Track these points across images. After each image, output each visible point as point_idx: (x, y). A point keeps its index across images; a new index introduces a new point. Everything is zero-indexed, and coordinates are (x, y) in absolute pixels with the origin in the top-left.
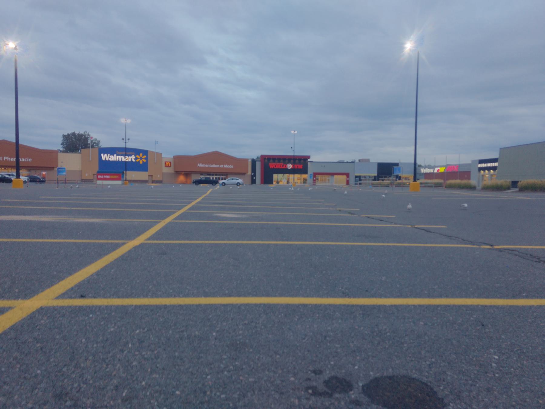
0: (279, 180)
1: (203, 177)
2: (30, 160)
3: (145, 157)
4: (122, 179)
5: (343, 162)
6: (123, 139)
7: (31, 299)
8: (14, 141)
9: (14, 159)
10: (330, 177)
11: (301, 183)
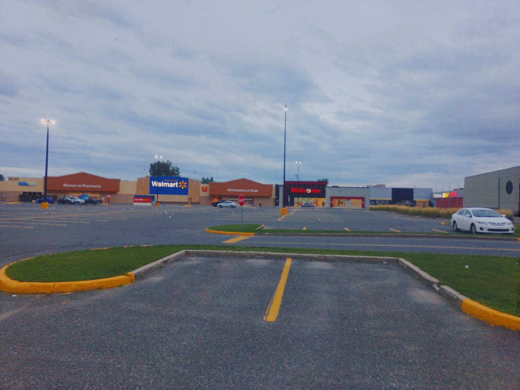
2: (100, 187)
3: (186, 183)
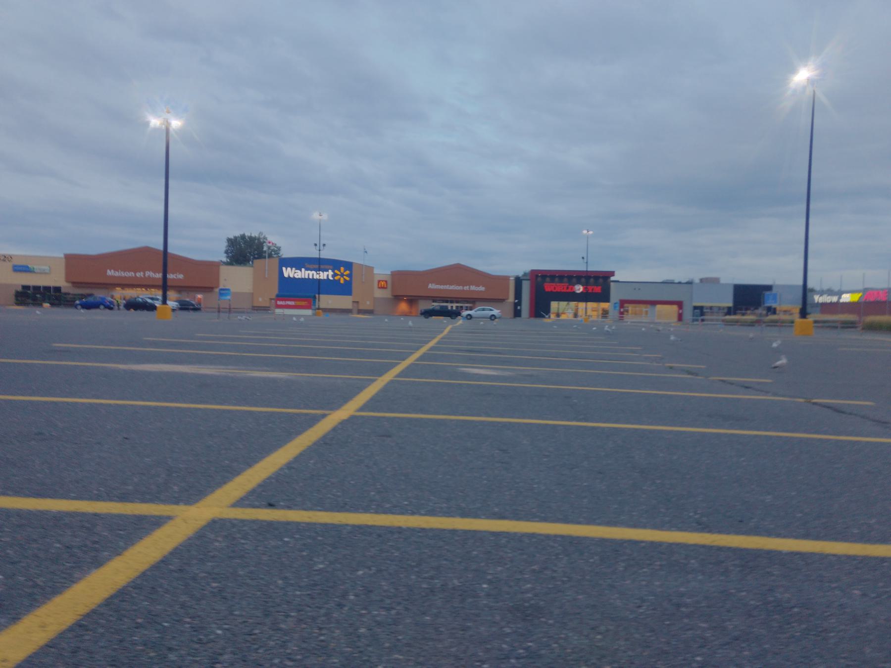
0: (561, 311)
1: (436, 305)
2: (181, 276)
3: (347, 272)
4: (313, 307)
5: (672, 283)
6: (316, 245)
7: (198, 505)
8: (161, 248)
9: (159, 276)
10: (649, 308)
11: (598, 316)
